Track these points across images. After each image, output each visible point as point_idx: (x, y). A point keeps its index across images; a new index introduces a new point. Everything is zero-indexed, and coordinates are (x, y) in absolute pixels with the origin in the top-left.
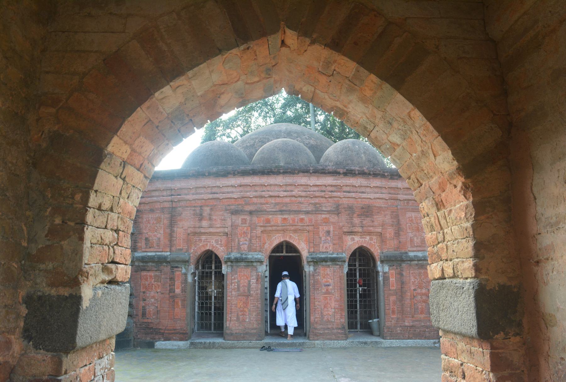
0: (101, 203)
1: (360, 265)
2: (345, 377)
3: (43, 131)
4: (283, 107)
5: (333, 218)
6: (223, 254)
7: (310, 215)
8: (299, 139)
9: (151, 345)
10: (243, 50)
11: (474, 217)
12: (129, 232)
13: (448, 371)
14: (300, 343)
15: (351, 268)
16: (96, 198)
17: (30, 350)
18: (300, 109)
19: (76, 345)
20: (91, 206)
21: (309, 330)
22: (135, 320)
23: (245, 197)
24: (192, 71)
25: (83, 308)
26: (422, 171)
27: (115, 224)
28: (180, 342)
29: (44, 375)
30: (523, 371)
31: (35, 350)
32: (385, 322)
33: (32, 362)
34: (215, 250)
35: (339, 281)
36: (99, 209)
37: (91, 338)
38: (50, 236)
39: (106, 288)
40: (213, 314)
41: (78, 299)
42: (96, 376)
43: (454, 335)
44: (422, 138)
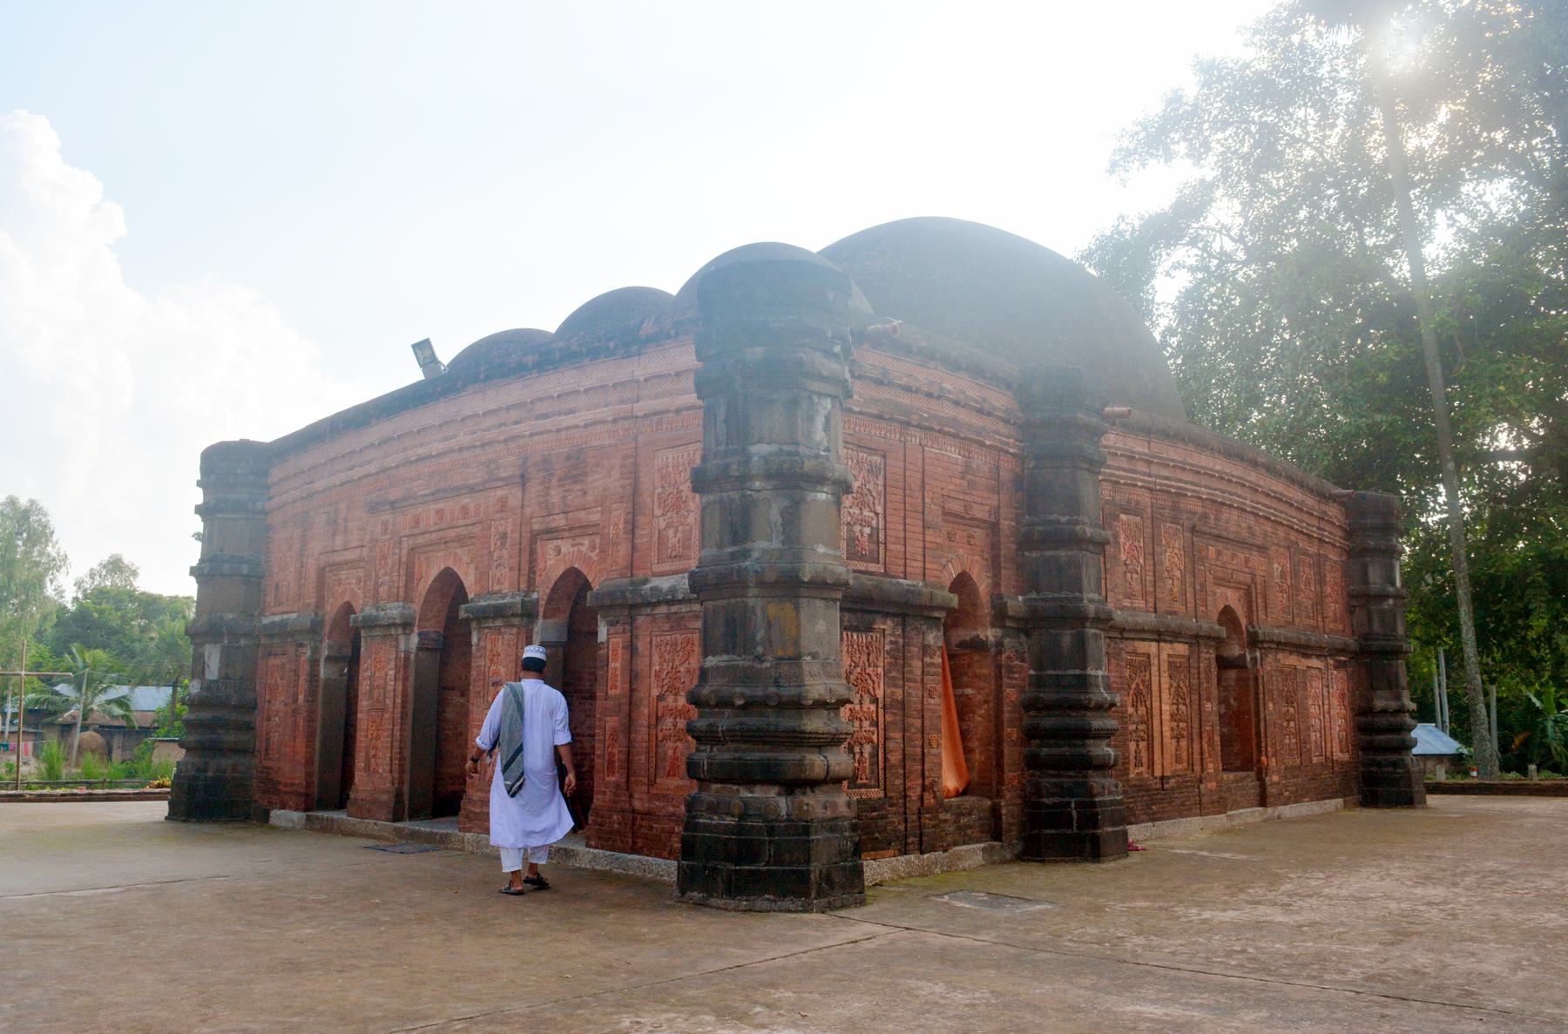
9: (263, 818)
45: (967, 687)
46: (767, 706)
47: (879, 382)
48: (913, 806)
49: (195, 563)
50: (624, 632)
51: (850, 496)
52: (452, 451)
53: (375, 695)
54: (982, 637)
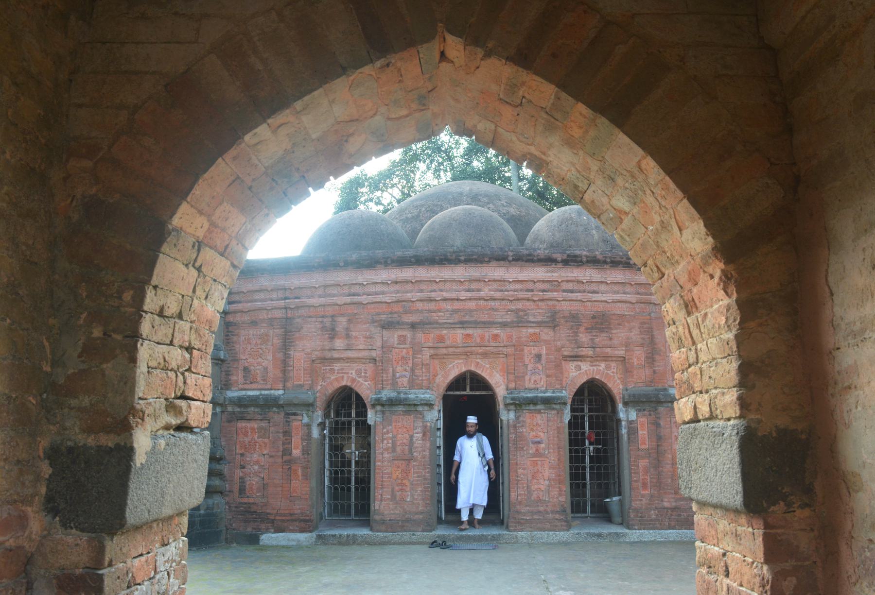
0: (163, 305)
1: (590, 410)
2: (565, 589)
3: (74, 196)
4: (467, 155)
5: (547, 334)
6: (368, 392)
7: (508, 330)
8: (491, 206)
9: (253, 540)
10: (380, 68)
11: (740, 324)
12: (208, 351)
13: (705, 566)
14: (493, 536)
15: (576, 414)
16: (155, 298)
17: (56, 530)
18: (494, 158)
19: (126, 521)
20: (148, 310)
21: (509, 514)
22: (227, 499)
23: (404, 301)
24: (300, 101)
25: (135, 465)
26: (664, 254)
27: (186, 338)
28: (301, 534)
29: (77, 567)
30: (815, 562)
31: (63, 529)
32: (631, 502)
33: (60, 547)
34: (355, 386)
35: (556, 436)
36: (161, 314)
37: (149, 512)
38: (85, 355)
39: (172, 437)
40: (353, 490)
41: (128, 452)
42: (158, 573)
43: (713, 509)
44: (660, 201)
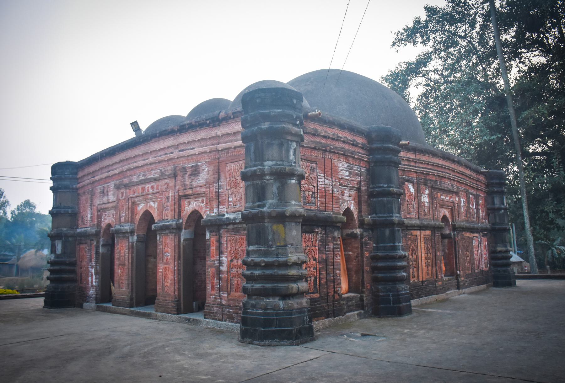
45: (350, 251)
46: (274, 265)
47: (314, 135)
48: (331, 299)
49: (50, 209)
50: (216, 235)
51: (304, 180)
52: (147, 164)
53: (121, 259)
54: (355, 232)
